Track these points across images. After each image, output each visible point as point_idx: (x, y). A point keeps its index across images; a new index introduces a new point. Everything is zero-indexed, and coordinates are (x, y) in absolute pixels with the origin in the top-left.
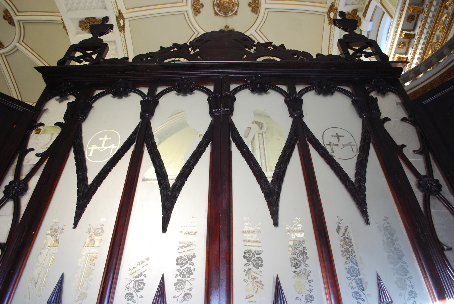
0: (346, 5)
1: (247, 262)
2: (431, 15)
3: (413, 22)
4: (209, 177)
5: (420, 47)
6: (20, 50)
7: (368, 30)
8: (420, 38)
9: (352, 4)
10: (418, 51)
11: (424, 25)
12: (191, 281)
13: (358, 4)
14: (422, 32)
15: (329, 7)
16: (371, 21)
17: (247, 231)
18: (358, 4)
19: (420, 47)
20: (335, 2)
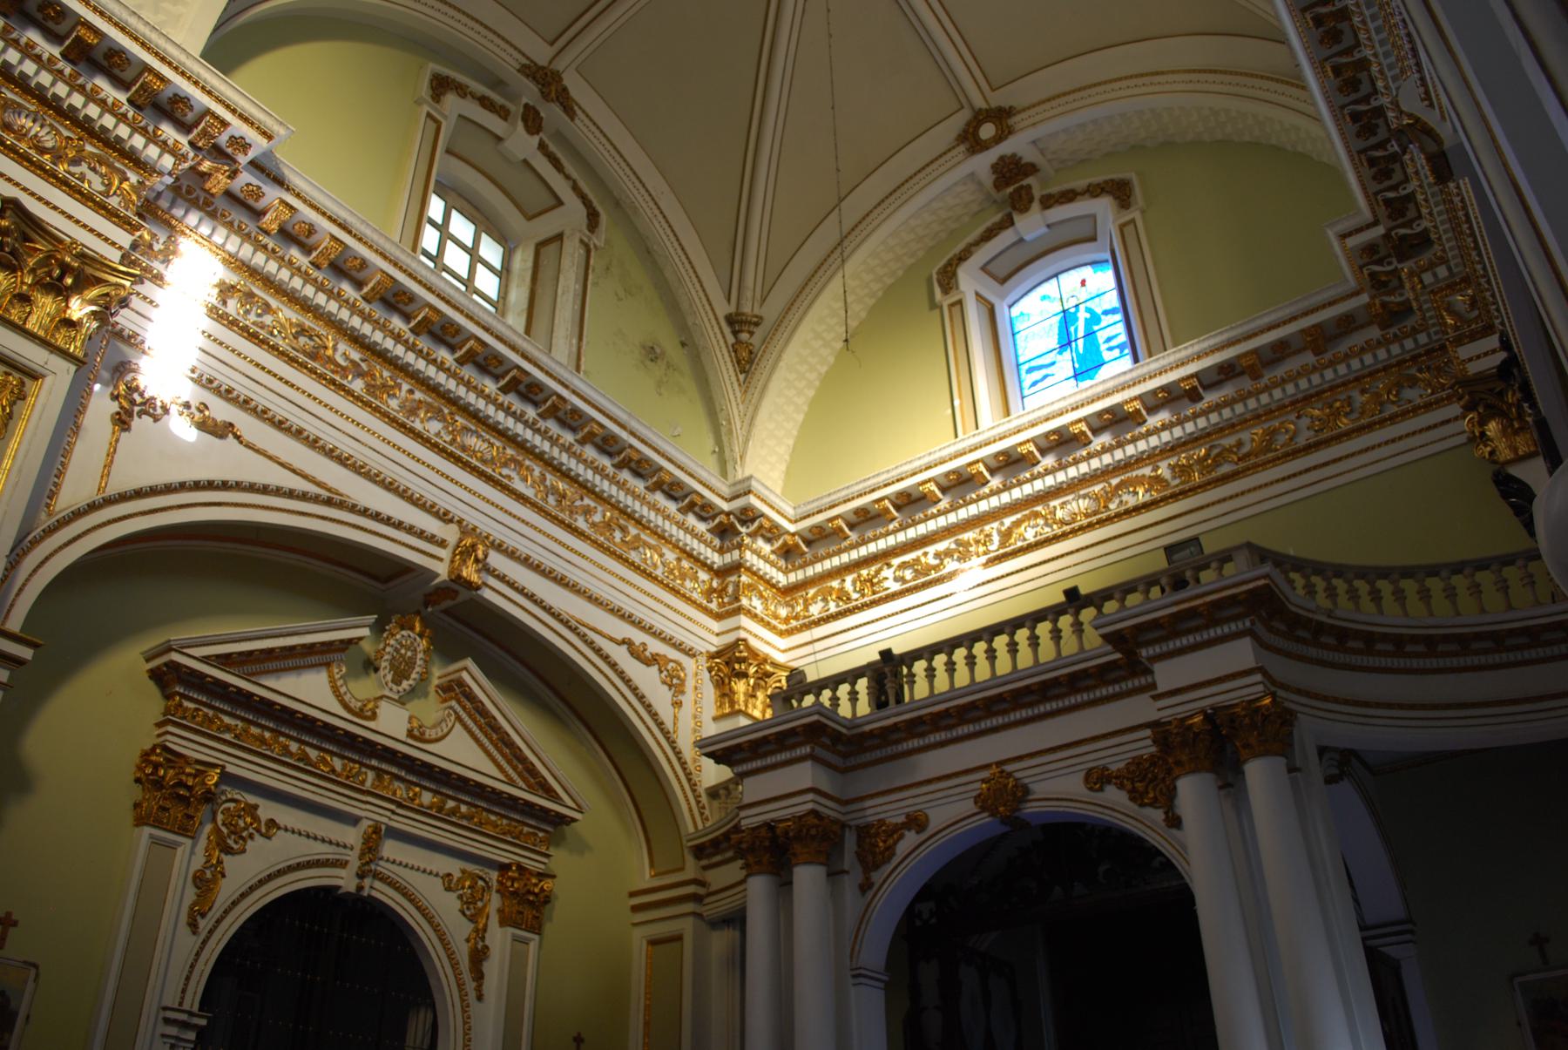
0: (1034, 142)
1: (656, 667)
2: (1264, 398)
3: (1222, 377)
4: (522, 622)
5: (1190, 427)
6: (1161, 355)
7: (1025, 238)
8: (1205, 413)
9: (1042, 152)
10: (1177, 432)
11: (1229, 403)
12: (437, 692)
13: (1049, 161)
14: (1217, 408)
15: (994, 104)
16: (1049, 226)
17: (663, 636)
18: (1049, 161)
19: (1190, 427)
20: (1019, 112)
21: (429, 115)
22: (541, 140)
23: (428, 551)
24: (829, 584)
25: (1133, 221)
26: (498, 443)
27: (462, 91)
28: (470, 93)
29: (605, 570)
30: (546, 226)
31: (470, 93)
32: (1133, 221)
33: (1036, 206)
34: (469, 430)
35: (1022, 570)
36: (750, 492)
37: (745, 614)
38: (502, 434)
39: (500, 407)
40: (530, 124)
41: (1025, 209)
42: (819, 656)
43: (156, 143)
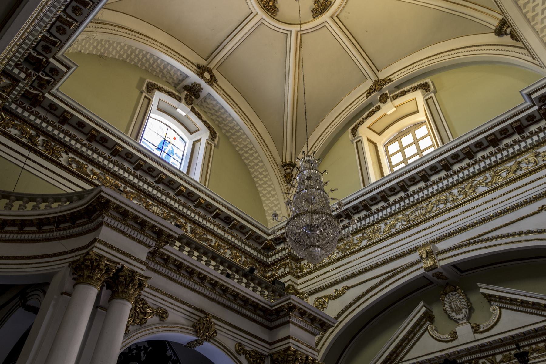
16: (396, 107)
21: (146, 97)
22: (192, 106)
23: (122, 258)
24: (538, 151)
25: (431, 97)
26: (166, 211)
27: (160, 89)
28: (164, 90)
29: (307, 281)
30: (196, 137)
31: (164, 90)
32: (431, 97)
33: (389, 100)
34: (153, 205)
35: (412, 241)
36: (288, 337)
37: (98, 242)
38: (165, 205)
39: (176, 201)
40: (188, 100)
41: (385, 102)
42: (26, 167)
43: (96, 153)
